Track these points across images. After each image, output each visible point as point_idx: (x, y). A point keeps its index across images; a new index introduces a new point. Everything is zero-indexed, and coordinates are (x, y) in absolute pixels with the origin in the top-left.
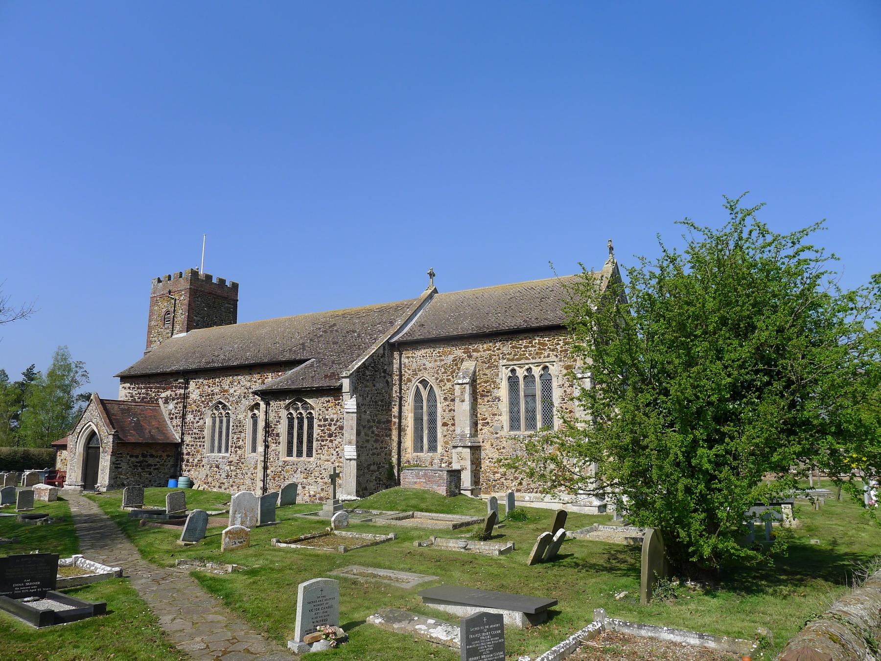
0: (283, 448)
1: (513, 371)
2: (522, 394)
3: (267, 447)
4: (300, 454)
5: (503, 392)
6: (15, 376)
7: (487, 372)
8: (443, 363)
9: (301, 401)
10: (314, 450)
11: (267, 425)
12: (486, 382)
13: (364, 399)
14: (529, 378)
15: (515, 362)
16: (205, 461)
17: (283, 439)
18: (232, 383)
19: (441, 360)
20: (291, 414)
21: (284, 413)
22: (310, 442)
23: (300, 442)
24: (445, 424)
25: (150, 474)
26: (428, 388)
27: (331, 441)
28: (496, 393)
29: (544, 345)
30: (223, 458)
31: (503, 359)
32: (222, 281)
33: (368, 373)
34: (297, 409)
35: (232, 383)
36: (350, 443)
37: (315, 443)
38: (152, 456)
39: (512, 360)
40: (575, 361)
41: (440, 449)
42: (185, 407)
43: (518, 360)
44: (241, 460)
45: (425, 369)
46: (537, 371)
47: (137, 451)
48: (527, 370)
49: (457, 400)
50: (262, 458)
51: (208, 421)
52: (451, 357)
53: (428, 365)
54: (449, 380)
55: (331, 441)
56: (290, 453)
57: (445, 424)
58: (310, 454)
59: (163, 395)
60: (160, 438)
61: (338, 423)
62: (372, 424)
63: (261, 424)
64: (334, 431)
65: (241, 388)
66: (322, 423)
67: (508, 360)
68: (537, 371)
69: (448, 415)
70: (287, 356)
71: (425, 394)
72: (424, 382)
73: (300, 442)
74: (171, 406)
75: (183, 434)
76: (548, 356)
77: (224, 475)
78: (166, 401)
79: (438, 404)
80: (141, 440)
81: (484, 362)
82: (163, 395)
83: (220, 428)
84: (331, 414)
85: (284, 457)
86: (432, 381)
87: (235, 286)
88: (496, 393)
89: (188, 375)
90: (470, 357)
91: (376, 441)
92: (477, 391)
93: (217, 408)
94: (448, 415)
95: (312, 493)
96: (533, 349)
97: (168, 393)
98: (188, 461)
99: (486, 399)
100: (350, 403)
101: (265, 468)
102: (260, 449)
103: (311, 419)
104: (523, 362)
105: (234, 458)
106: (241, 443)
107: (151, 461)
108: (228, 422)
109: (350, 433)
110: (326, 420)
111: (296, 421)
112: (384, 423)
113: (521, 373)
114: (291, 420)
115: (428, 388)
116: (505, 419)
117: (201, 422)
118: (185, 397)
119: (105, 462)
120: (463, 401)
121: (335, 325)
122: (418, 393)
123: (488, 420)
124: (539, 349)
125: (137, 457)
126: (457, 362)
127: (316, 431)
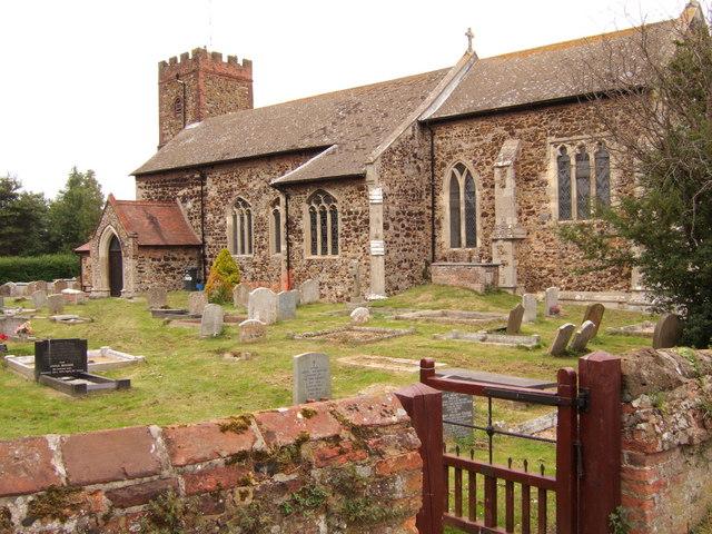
0: (307, 245)
3: (289, 245)
4: (324, 251)
7: (533, 151)
8: (481, 143)
12: (531, 163)
15: (565, 139)
17: (307, 235)
18: (250, 176)
20: (312, 208)
21: (305, 208)
22: (334, 238)
25: (174, 278)
26: (465, 173)
30: (248, 259)
31: (551, 135)
33: (395, 158)
34: (318, 202)
35: (250, 176)
37: (340, 240)
38: (174, 259)
39: (562, 136)
41: (479, 243)
42: (203, 205)
44: (265, 261)
46: (592, 151)
47: (159, 254)
49: (497, 186)
50: (286, 258)
51: (229, 220)
52: (490, 136)
53: (465, 146)
54: (488, 163)
56: (314, 251)
58: (335, 252)
59: (181, 193)
61: (364, 217)
62: (401, 216)
65: (257, 180)
66: (346, 217)
68: (592, 151)
70: (306, 143)
71: (461, 181)
72: (460, 167)
75: (203, 235)
79: (477, 192)
82: (181, 193)
84: (356, 206)
85: (308, 256)
86: (469, 164)
87: (247, 64)
88: (543, 176)
89: (204, 170)
90: (512, 134)
91: (408, 235)
92: (527, 175)
93: (237, 206)
95: (339, 293)
97: (185, 191)
101: (289, 268)
102: (283, 248)
103: (334, 212)
104: (574, 137)
105: (258, 259)
106: (264, 242)
107: (174, 264)
109: (376, 227)
110: (350, 213)
113: (571, 151)
114: (313, 214)
115: (465, 173)
116: (554, 206)
118: (203, 194)
119: (129, 266)
120: (504, 187)
125: (159, 260)
127: (341, 226)
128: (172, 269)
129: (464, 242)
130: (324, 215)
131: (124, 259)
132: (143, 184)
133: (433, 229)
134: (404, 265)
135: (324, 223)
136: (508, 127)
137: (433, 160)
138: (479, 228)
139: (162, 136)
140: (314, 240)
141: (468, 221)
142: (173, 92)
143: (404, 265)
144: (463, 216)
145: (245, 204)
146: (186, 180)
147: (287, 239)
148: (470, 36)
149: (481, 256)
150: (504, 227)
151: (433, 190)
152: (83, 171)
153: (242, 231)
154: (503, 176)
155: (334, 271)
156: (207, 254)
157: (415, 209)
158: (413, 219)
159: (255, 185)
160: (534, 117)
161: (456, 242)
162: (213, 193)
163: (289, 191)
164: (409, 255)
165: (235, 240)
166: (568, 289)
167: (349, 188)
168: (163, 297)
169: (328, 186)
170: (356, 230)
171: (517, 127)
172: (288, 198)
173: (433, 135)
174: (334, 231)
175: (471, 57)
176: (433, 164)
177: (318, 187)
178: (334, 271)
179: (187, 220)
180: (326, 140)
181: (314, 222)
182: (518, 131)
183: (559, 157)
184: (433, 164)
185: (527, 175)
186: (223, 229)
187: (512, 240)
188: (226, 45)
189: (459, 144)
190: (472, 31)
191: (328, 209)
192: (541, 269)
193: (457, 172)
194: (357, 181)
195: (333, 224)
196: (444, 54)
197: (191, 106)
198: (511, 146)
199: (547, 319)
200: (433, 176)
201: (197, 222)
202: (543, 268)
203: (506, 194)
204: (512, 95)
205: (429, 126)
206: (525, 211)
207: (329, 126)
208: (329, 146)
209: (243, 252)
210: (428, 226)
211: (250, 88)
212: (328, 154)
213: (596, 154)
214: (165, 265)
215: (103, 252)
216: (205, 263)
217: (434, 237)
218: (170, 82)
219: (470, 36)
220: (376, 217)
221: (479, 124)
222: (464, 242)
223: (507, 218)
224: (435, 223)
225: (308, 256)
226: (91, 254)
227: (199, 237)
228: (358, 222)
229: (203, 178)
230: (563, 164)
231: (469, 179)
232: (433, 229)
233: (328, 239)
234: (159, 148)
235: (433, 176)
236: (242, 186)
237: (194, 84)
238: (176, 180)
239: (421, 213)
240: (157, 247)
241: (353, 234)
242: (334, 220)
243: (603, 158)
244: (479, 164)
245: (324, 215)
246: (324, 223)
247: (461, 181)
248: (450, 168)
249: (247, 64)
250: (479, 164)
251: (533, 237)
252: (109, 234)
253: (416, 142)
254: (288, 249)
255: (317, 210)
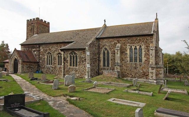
0: (69, 64)
1: (131, 47)
2: (133, 53)
3: (64, 64)
4: (74, 66)
5: (128, 52)
6: (15, 39)
7: (124, 47)
9: (73, 52)
10: (78, 65)
11: (64, 58)
12: (123, 49)
13: (91, 52)
14: (136, 49)
15: (132, 44)
16: (46, 67)
17: (69, 62)
18: (52, 47)
19: (111, 43)
20: (59, 56)
21: (69, 55)
22: (76, 63)
23: (74, 63)
24: (111, 60)
27: (83, 63)
28: (126, 52)
29: (140, 40)
30: (51, 66)
31: (128, 43)
32: (45, 22)
33: (92, 45)
34: (72, 54)
35: (52, 47)
36: (88, 63)
37: (78, 63)
39: (131, 44)
40: (149, 44)
41: (110, 66)
42: (39, 53)
43: (133, 44)
44: (55, 67)
45: (106, 45)
46: (138, 47)
47: (28, 64)
48: (135, 47)
49: (116, 54)
50: (63, 67)
51: (46, 57)
52: (113, 42)
53: (107, 44)
54: (113, 48)
55: (83, 63)
56: (71, 65)
57: (111, 60)
58: (76, 66)
59: (33, 50)
60: (36, 61)
61: (85, 58)
63: (63, 58)
64: (84, 60)
65: (53, 48)
66: (80, 58)
67: (130, 44)
68: (138, 47)
69: (112, 57)
70: (67, 41)
71: (106, 52)
72: (106, 49)
73: (74, 63)
74: (35, 53)
75: (39, 60)
76: (142, 43)
77: (51, 71)
78: (34, 51)
79: (110, 55)
80: (29, 61)
81: (123, 44)
82: (33, 50)
83: (49, 60)
84: (82, 56)
85: (69, 67)
86: (108, 48)
87: (49, 23)
88: (126, 52)
89: (40, 45)
90: (119, 43)
91: (93, 63)
92: (123, 52)
93: (48, 54)
94: (112, 57)
95: (77, 76)
96: (137, 41)
97: (34, 49)
98: (41, 67)
99: (123, 54)
100: (88, 53)
101: (64, 69)
102: (63, 64)
103: (76, 57)
104: (134, 44)
105: (53, 66)
106: (55, 63)
107: (31, 66)
108: (51, 57)
109: (88, 61)
110: (81, 57)
111: (75, 57)
112: (95, 59)
113: (133, 48)
114: (71, 57)
116: (128, 59)
117: (44, 57)
118: (39, 50)
119: (20, 66)
120: (118, 54)
121: (79, 33)
122: (104, 53)
123: (124, 59)
124: (139, 41)
125: (28, 65)
126: (115, 44)
127: (78, 60)
128: (31, 67)
129: (106, 65)
130: (74, 57)
131: (19, 64)
132: (23, 47)
133: (99, 62)
134: (93, 70)
135: (74, 59)
136: (118, 41)
137: (99, 47)
138: (110, 63)
139: (27, 37)
140: (71, 63)
141: (106, 60)
142: (30, 27)
143: (93, 70)
144: (106, 60)
145: (50, 53)
146: (35, 47)
147: (64, 62)
148: (105, 21)
149: (111, 69)
150: (118, 63)
151: (99, 54)
152: (5, 43)
153: (49, 60)
154: (118, 52)
155: (76, 71)
156: (40, 64)
157: (95, 58)
158: (95, 60)
159: (53, 49)
160: (124, 39)
161: (104, 65)
162: (42, 50)
163: (65, 51)
164: (94, 68)
165: (48, 62)
166: (132, 77)
167: (81, 51)
168: (33, 75)
169: (75, 51)
170: (82, 61)
171: (120, 41)
172: (64, 53)
173: (99, 41)
174: (76, 61)
175: (105, 26)
176: (99, 48)
177: (73, 50)
178: (76, 71)
179: (35, 56)
180: (72, 40)
181: (71, 59)
182: (120, 42)
183: (130, 48)
184: (99, 48)
185: (123, 52)
186: (44, 59)
187: (119, 66)
188: (44, 18)
189: (106, 44)
190: (106, 20)
191: (75, 56)
192: (125, 73)
193: (105, 50)
194: (84, 50)
195: (76, 59)
196: (100, 25)
197: (35, 30)
198: (119, 45)
199: (10, 75)
200: (99, 50)
201: (38, 57)
202: (126, 73)
203: (118, 55)
204: (118, 34)
205: (98, 39)
206: (122, 60)
207: (72, 37)
208: (73, 42)
209: (49, 64)
210: (97, 61)
211: (49, 28)
212: (74, 43)
213: (139, 48)
214: (29, 67)
215: (12, 62)
216: (39, 66)
217: (99, 64)
218: (30, 24)
219: (105, 21)
220: (88, 59)
221: (111, 40)
222: (106, 65)
223: (118, 61)
224: (99, 61)
225: (69, 67)
226: (9, 63)
227: (38, 60)
228: (83, 59)
229: (39, 47)
230: (131, 49)
231: (108, 53)
232: (99, 62)
233: (74, 62)
234: (26, 39)
235: (99, 50)
236: (50, 49)
237: (37, 26)
238: (32, 47)
239: (96, 59)
240: (27, 62)
241: (82, 62)
242: (77, 59)
243: (141, 49)
244: (111, 49)
245: (74, 57)
246: (74, 59)
247: (106, 52)
248: (103, 49)
249: (49, 23)
250: (111, 49)
251: (123, 66)
252: (14, 58)
253: (95, 42)
254: (64, 64)
255: (72, 56)
